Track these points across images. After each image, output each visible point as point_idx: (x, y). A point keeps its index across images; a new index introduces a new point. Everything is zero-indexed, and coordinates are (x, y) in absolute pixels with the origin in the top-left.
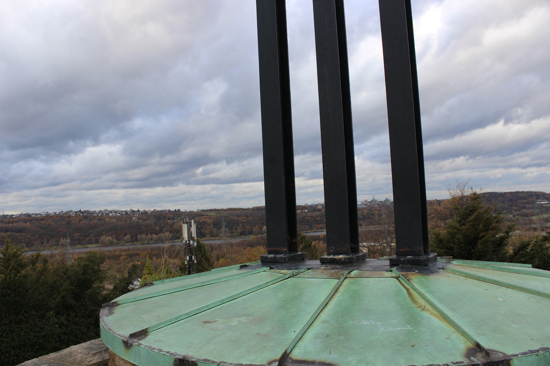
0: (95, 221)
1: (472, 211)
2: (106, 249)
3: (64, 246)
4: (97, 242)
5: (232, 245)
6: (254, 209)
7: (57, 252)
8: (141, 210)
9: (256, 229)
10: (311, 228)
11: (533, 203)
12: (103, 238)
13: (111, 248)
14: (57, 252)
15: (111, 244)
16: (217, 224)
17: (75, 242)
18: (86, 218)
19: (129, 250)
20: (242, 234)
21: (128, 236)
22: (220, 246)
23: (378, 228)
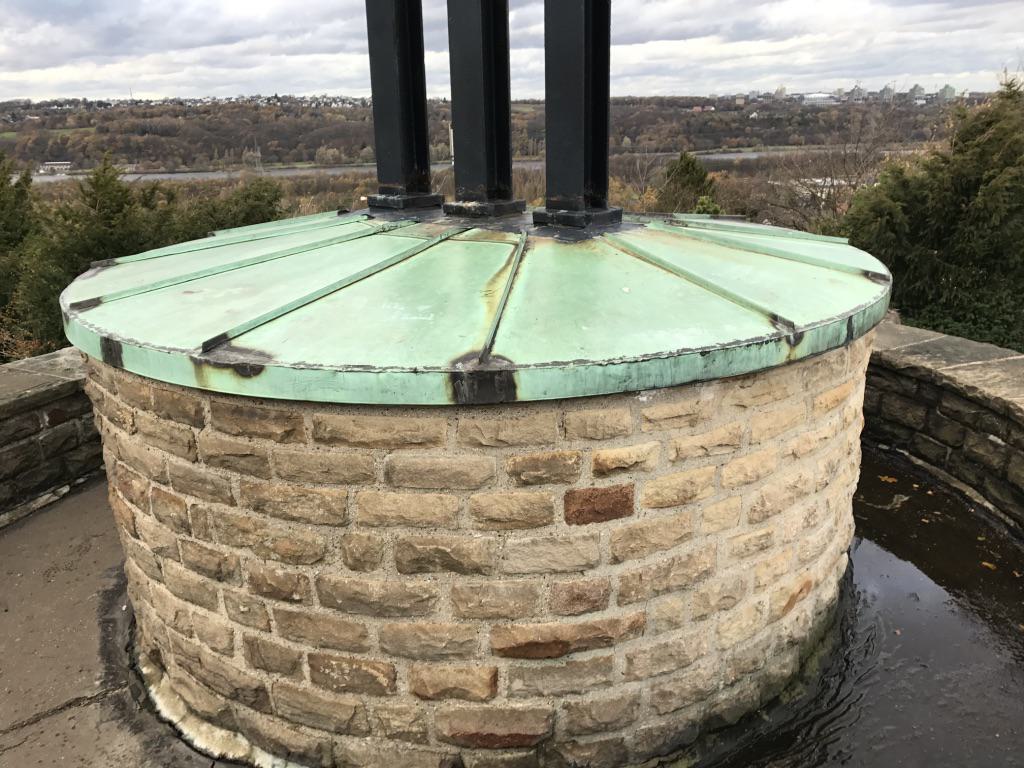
0: (306, 118)
2: (330, 172)
3: (251, 163)
4: (311, 158)
10: (717, 145)
12: (322, 149)
13: (338, 172)
15: (337, 162)
18: (287, 110)
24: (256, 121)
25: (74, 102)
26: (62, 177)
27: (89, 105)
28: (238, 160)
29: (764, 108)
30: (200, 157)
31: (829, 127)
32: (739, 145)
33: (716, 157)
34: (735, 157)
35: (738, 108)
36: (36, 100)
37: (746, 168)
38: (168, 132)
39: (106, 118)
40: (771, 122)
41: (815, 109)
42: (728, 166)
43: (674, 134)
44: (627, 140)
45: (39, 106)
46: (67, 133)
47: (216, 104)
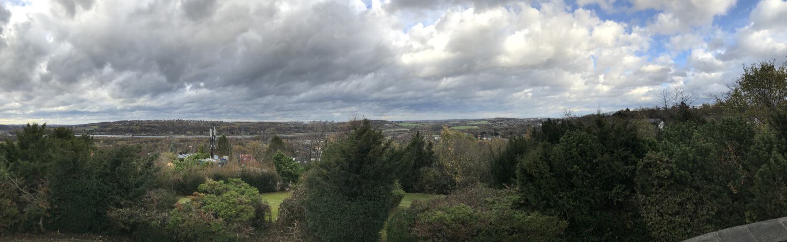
0: (185, 125)
1: (365, 131)
2: (189, 137)
3: (171, 134)
4: (185, 134)
5: (246, 139)
6: (257, 123)
7: (167, 137)
8: (205, 120)
9: (258, 132)
10: (285, 133)
11: (383, 125)
12: (188, 132)
13: (191, 137)
14: (167, 137)
15: (191, 135)
16: (240, 129)
17: (176, 133)
18: (181, 123)
19: (198, 138)
20: (251, 134)
21: (198, 132)
22: (241, 139)
23: (314, 134)
24: (173, 125)
25: (136, 121)
26: (131, 136)
27: (139, 121)
28: (168, 133)
29: (294, 125)
30: (160, 132)
31: (310, 129)
32: (290, 133)
33: (285, 136)
34: (289, 136)
35: (289, 125)
36: (129, 120)
37: (292, 138)
38: (154, 127)
39: (142, 124)
40: (297, 128)
41: (306, 125)
42: (287, 138)
43: (273, 130)
44: (262, 132)
45: (129, 121)
46: (134, 127)
47: (165, 121)
